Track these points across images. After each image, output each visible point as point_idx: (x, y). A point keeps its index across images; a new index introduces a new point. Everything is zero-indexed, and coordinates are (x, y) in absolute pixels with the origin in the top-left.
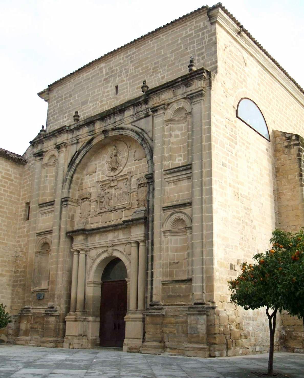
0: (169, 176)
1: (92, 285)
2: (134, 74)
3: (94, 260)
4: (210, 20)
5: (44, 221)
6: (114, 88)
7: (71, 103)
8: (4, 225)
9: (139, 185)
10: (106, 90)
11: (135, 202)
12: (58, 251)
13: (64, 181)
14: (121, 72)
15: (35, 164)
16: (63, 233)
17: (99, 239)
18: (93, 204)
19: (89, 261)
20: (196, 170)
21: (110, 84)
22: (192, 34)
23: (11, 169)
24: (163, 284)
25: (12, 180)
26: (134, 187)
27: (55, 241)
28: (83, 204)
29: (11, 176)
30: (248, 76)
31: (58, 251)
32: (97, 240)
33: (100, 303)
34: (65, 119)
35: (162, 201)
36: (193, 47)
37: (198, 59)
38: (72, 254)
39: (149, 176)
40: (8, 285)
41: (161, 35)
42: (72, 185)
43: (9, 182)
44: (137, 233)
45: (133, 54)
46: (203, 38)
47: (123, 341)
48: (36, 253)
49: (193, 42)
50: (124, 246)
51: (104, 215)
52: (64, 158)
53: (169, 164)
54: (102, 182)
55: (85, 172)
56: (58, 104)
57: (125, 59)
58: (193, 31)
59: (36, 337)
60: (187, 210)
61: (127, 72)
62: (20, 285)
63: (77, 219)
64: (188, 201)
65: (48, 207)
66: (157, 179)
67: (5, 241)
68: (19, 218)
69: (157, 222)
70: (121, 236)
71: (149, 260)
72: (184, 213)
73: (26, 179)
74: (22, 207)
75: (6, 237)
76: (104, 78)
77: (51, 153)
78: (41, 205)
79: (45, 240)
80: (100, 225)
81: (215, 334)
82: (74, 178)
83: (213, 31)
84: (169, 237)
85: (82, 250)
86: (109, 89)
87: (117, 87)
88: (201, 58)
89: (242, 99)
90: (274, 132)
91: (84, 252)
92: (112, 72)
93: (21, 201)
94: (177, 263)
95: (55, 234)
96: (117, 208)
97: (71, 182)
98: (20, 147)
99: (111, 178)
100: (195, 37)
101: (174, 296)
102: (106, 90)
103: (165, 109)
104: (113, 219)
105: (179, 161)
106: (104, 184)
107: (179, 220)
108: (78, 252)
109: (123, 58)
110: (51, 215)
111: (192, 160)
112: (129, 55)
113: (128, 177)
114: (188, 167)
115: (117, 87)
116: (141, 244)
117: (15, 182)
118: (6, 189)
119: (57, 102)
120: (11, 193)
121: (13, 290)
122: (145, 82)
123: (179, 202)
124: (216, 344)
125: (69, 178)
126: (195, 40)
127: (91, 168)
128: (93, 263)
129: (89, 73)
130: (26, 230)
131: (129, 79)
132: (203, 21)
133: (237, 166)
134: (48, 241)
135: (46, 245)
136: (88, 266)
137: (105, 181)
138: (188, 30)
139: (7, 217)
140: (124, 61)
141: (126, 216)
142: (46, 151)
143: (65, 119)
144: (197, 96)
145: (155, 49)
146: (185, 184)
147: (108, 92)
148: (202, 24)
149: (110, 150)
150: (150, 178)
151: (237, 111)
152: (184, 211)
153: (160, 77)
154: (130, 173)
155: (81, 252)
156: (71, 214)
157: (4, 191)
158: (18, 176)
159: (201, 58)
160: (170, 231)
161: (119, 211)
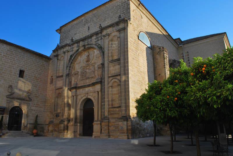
6: (87, 27)
7: (70, 34)
13: (67, 67)
20: (122, 61)
21: (86, 26)
23: (45, 62)
26: (96, 69)
35: (108, 74)
36: (121, 10)
39: (102, 64)
44: (98, 87)
46: (124, 7)
49: (120, 8)
56: (65, 35)
58: (120, 4)
59: (56, 133)
61: (93, 21)
62: (49, 111)
63: (73, 83)
66: (106, 65)
69: (106, 83)
70: (91, 88)
71: (103, 98)
82: (71, 66)
83: (129, 3)
86: (86, 28)
87: (89, 27)
100: (121, 6)
101: (113, 114)
102: (84, 29)
104: (88, 82)
111: (120, 56)
115: (89, 27)
116: (74, 97)
119: (64, 34)
123: (115, 74)
126: (121, 7)
128: (79, 101)
131: (94, 24)
136: (78, 102)
138: (118, 3)
143: (67, 41)
145: (105, 11)
147: (85, 29)
150: (103, 64)
158: (48, 65)
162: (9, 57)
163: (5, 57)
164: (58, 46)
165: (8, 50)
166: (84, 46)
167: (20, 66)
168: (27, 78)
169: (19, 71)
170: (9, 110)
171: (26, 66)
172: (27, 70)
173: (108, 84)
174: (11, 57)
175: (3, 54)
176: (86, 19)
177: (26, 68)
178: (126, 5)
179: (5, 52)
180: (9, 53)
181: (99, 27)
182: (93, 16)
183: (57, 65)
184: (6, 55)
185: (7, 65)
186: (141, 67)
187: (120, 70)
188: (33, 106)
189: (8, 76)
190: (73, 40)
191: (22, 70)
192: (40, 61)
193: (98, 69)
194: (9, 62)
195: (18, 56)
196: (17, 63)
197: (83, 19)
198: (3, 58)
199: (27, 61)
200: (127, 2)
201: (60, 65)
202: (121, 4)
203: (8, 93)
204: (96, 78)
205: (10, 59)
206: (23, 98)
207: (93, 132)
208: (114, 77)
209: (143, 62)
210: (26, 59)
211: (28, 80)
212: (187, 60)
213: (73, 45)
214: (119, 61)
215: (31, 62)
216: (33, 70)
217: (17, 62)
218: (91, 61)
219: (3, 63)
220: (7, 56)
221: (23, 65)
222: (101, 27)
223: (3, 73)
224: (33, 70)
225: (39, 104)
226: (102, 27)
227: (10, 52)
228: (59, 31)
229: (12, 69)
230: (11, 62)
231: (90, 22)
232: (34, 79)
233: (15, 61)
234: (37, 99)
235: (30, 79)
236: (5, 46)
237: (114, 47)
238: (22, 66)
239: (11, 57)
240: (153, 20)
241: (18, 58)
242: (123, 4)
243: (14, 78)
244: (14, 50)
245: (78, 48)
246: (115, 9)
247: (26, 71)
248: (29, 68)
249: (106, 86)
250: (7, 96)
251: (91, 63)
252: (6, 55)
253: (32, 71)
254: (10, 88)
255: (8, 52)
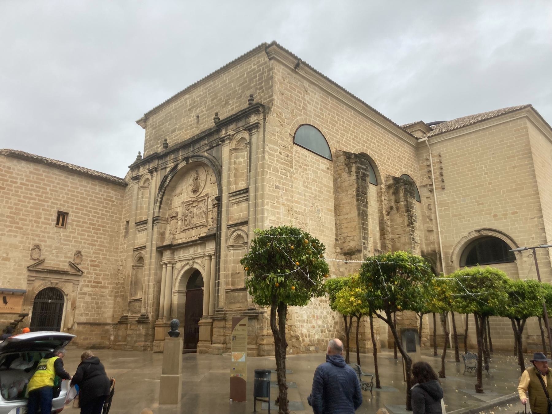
0: (233, 198)
1: (177, 294)
2: (211, 105)
3: (179, 272)
4: (268, 56)
5: (141, 238)
6: (195, 117)
8: (107, 243)
9: (214, 205)
10: (190, 120)
11: (210, 220)
12: (150, 265)
13: (156, 201)
14: (201, 103)
15: (134, 186)
16: (154, 249)
17: (183, 253)
18: (179, 222)
19: (176, 272)
20: (252, 194)
21: (193, 114)
22: (255, 69)
23: (112, 192)
24: (226, 292)
25: (114, 202)
26: (210, 207)
27: (148, 256)
28: (172, 222)
29: (112, 197)
30: (309, 103)
31: (150, 265)
32: (183, 254)
33: (184, 310)
34: (158, 146)
35: (227, 220)
36: (256, 81)
37: (259, 93)
38: (161, 266)
40: (110, 296)
41: (231, 70)
42: (162, 206)
43: (111, 203)
44: (210, 248)
45: (211, 86)
46: (263, 73)
47: (197, 343)
48: (133, 266)
50: (201, 259)
51: (187, 231)
52: (156, 181)
53: (233, 188)
54: (186, 202)
55: (174, 194)
57: (204, 91)
58: (256, 66)
60: (244, 228)
61: (206, 103)
62: (121, 295)
63: (167, 235)
64: (246, 220)
65: (143, 226)
66: (224, 201)
67: (108, 257)
68: (121, 235)
69: (223, 238)
70: (199, 250)
72: (242, 231)
73: (127, 199)
74: (123, 226)
75: (108, 253)
76: (188, 108)
77: (146, 177)
78: (138, 224)
79: (140, 255)
80: (184, 241)
81: (263, 336)
84: (232, 251)
85: (169, 263)
86: (192, 118)
87: (198, 117)
88: (261, 91)
89: (301, 125)
90: (337, 151)
91: (171, 265)
92: (195, 102)
93: (122, 220)
94: (239, 273)
95: (148, 249)
96: (197, 225)
97: (161, 203)
98: (121, 172)
99: (193, 199)
102: (190, 120)
103: (231, 140)
104: (194, 234)
105: (242, 185)
106: (188, 204)
107: (240, 236)
108: (166, 264)
109: (203, 91)
110: (145, 233)
111: (249, 185)
112: (208, 88)
113: (206, 198)
114: (246, 191)
115: (198, 117)
116: (213, 257)
117: (117, 203)
118: (108, 210)
120: (112, 213)
121: (115, 300)
122: (216, 114)
123: (240, 221)
124: (263, 345)
125: (159, 199)
127: (178, 191)
128: (178, 274)
129: (176, 104)
130: (126, 246)
132: (263, 58)
133: (292, 187)
134: (142, 256)
135: (141, 259)
136: (175, 277)
137: (189, 201)
138: (252, 65)
139: (109, 235)
140: (204, 93)
141: (203, 232)
142: (142, 175)
143: (158, 146)
144: (254, 127)
145: (227, 82)
146: (244, 205)
148: (262, 59)
149: (193, 175)
150: (219, 199)
151: (294, 137)
152: (242, 228)
153: (230, 108)
154: (207, 194)
155: (168, 265)
156: (161, 231)
157: (106, 211)
158: (119, 197)
159: (261, 91)
160: (232, 246)
161: (199, 228)
162: (32, 186)
163: (24, 187)
164: (139, 156)
165: (31, 172)
166: (186, 159)
167: (57, 204)
168: (74, 227)
169: (56, 214)
170: (35, 295)
171: (72, 203)
172: (73, 212)
173: (227, 240)
174: (37, 187)
175: (19, 181)
176: (193, 100)
177: (72, 208)
178: (266, 70)
179: (23, 177)
180: (33, 178)
181: (214, 119)
182: (206, 93)
183: (138, 198)
184: (27, 183)
185: (29, 203)
186: (297, 202)
187: (249, 213)
188: (88, 286)
189: (32, 226)
190: (167, 144)
191: (62, 210)
192: (103, 189)
193: (213, 208)
194: (34, 196)
195: (53, 182)
196: (50, 199)
197: (186, 99)
198: (20, 191)
199: (74, 192)
200: (268, 64)
201: (143, 198)
202: (258, 67)
203: (32, 261)
204: (209, 227)
205: (35, 191)
206: (65, 270)
207: (198, 341)
208: (239, 228)
209: (304, 190)
210: (71, 187)
211: (77, 231)
212: (438, 173)
213: (166, 155)
214: (247, 195)
215: (82, 194)
216: (86, 211)
217: (50, 196)
218: (200, 190)
219: (19, 201)
220: (30, 184)
221: (64, 201)
222: (217, 120)
223: (21, 219)
224: (86, 211)
225: (101, 280)
226: (219, 119)
227: (35, 176)
228: (144, 121)
229: (41, 211)
230: (37, 197)
231: (201, 106)
232: (89, 228)
233: (47, 193)
234: (96, 270)
235: (80, 229)
236: (23, 164)
237: (240, 163)
238: (62, 202)
239: (37, 187)
240: (338, 91)
241: (54, 186)
242: (261, 68)
243: (45, 228)
244: (44, 171)
245: (176, 163)
246: (246, 77)
247: (70, 213)
248: (79, 207)
249: (223, 245)
250: (28, 267)
251: (200, 196)
252: (27, 183)
253: (84, 212)
254: (37, 250)
255: (32, 176)
